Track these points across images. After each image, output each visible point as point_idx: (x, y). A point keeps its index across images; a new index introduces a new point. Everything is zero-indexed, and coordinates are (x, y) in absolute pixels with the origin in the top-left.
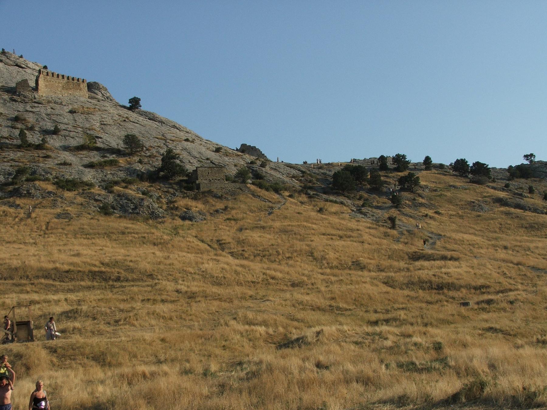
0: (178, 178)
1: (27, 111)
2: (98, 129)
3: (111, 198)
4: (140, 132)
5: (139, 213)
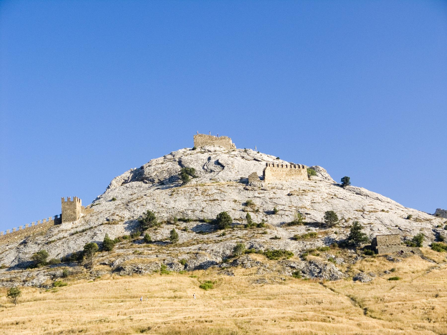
0: (363, 246)
1: (255, 197)
2: (309, 207)
3: (303, 265)
4: (344, 207)
5: (322, 276)
